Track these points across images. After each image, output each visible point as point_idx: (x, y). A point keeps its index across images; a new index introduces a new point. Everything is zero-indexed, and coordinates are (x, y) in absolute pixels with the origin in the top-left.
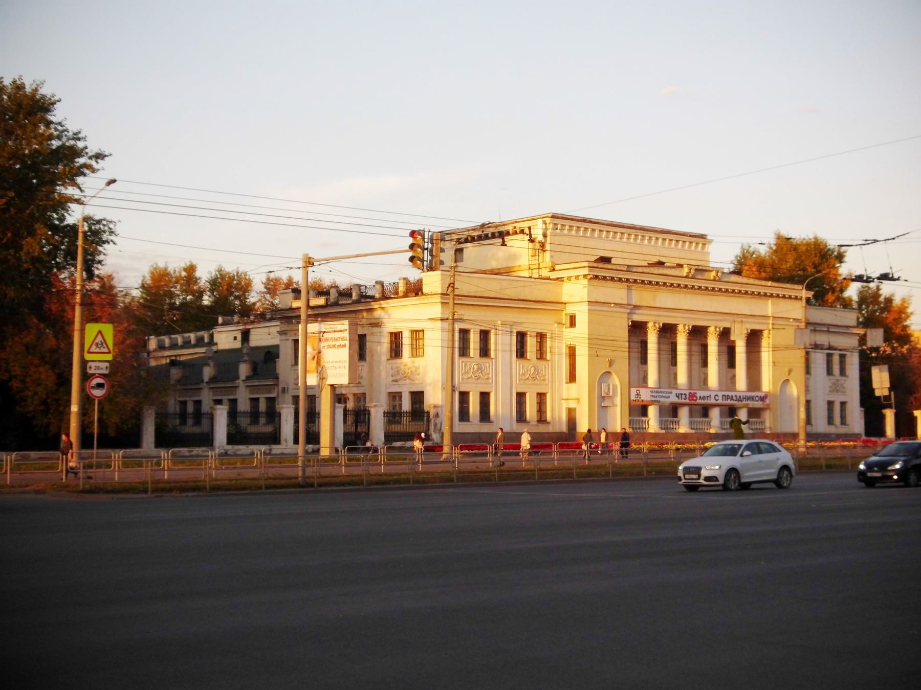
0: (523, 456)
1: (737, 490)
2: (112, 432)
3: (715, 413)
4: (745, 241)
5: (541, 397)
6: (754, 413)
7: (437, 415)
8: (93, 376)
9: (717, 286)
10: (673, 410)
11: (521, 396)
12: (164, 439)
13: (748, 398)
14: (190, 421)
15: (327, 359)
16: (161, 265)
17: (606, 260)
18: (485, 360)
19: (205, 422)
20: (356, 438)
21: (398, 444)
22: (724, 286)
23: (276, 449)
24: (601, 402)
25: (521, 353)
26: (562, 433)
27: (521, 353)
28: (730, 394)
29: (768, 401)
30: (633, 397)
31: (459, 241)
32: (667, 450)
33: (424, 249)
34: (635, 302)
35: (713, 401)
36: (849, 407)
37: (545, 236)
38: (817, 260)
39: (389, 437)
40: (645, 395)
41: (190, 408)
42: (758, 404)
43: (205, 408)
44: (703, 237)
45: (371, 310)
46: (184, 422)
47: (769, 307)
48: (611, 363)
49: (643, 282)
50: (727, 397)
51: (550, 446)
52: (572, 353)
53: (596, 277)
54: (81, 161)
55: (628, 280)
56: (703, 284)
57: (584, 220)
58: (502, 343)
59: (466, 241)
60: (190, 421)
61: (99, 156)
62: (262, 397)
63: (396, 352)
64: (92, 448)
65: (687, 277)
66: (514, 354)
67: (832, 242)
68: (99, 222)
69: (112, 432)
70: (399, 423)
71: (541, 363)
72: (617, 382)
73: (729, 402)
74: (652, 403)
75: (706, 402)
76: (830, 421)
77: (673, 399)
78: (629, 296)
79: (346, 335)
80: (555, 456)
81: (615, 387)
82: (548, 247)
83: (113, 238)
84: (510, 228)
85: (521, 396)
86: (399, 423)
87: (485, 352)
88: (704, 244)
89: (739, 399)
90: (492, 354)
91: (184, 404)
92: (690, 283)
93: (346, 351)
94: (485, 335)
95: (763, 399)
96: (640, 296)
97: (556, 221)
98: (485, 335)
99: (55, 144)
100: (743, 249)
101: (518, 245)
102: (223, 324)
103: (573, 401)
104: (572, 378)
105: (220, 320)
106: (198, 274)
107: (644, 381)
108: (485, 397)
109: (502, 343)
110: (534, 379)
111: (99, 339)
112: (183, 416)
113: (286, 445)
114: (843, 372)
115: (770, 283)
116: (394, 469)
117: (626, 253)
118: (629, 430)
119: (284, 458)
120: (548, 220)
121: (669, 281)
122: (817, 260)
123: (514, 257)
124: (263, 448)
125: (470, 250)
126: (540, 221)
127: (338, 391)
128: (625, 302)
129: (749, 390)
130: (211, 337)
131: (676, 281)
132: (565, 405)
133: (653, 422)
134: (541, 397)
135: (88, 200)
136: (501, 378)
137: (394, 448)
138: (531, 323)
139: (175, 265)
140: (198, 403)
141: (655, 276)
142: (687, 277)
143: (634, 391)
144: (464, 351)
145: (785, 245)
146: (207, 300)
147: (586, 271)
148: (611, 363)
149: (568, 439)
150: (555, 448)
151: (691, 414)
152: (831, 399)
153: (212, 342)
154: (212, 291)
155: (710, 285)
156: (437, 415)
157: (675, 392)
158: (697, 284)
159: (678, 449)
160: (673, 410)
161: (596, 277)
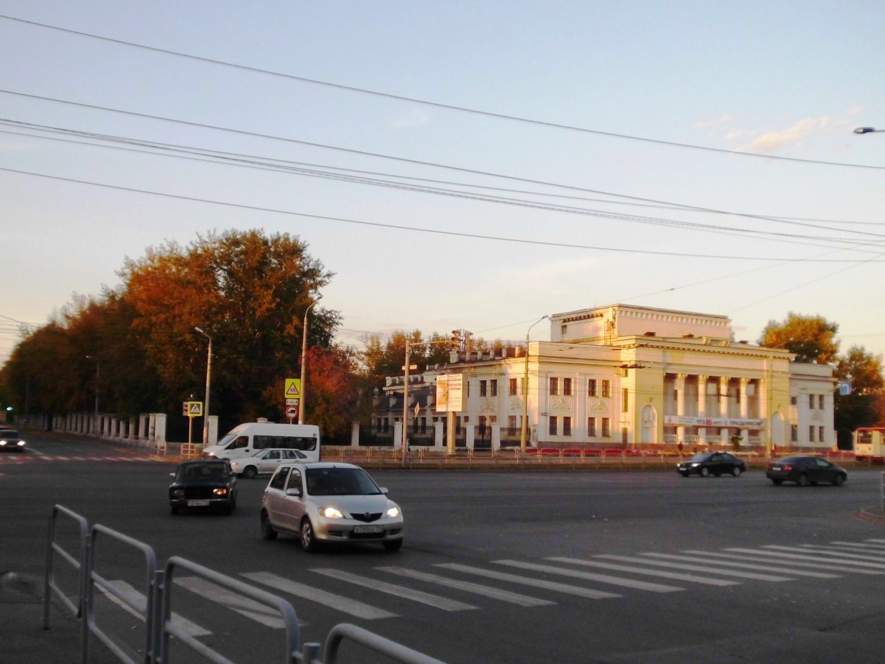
0: (470, 454)
1: (807, 486)
2: (332, 436)
3: (725, 433)
4: (772, 318)
5: (605, 421)
6: (753, 433)
7: (535, 431)
8: (289, 406)
9: (726, 350)
10: (695, 430)
11: (591, 420)
12: (365, 440)
13: (750, 423)
14: (420, 431)
15: (451, 394)
16: (400, 331)
17: (651, 334)
18: (567, 397)
19: (390, 431)
20: (483, 445)
21: (508, 448)
22: (731, 351)
23: (432, 449)
24: (643, 423)
25: (592, 393)
26: (619, 444)
27: (592, 393)
28: (736, 420)
29: (762, 425)
30: (666, 421)
31: (565, 321)
32: (659, 455)
33: (460, 340)
34: (669, 360)
35: (723, 425)
36: (825, 431)
37: (614, 318)
38: (816, 331)
39: (504, 443)
40: (675, 421)
41: (383, 423)
42: (755, 427)
43: (390, 423)
44: (724, 318)
45: (500, 365)
46: (379, 430)
47: (764, 364)
48: (651, 400)
49: (673, 348)
50: (734, 423)
51: (579, 451)
52: (626, 392)
53: (642, 346)
54: (319, 279)
55: (663, 347)
56: (716, 350)
57: (641, 308)
58: (579, 387)
59: (569, 320)
60: (420, 431)
61: (329, 275)
62: (383, 418)
63: (513, 391)
64: (187, 441)
65: (705, 345)
66: (587, 393)
67: (830, 320)
68: (330, 312)
69: (332, 436)
70: (514, 435)
71: (606, 400)
72: (655, 411)
73: (735, 425)
74: (680, 425)
75: (719, 425)
76: (812, 439)
77: (696, 424)
78: (664, 356)
79: (461, 382)
80: (582, 457)
81: (654, 415)
82: (616, 325)
83: (341, 321)
84: (594, 313)
85: (591, 420)
86: (514, 435)
87: (567, 391)
88: (726, 323)
89: (742, 424)
90: (572, 393)
91: (379, 420)
92: (707, 348)
93: (461, 391)
94: (568, 381)
95: (759, 424)
96: (671, 357)
97: (622, 309)
98: (568, 381)
99: (306, 268)
100: (770, 323)
101: (601, 322)
102: (430, 370)
103: (624, 422)
104: (626, 409)
105: (427, 368)
106: (421, 337)
107: (675, 412)
108: (567, 420)
109: (579, 387)
110: (601, 409)
111: (293, 387)
112: (379, 427)
113: (438, 447)
114: (821, 406)
115: (765, 349)
116: (474, 462)
117: (663, 330)
118: (683, 443)
119: (436, 455)
120: (616, 308)
121: (692, 347)
122: (816, 331)
123: (597, 329)
124: (424, 448)
125: (571, 326)
126: (611, 309)
127: (457, 415)
128: (661, 361)
129: (749, 417)
130: (422, 378)
131: (697, 348)
132: (622, 426)
133: (680, 437)
134: (605, 421)
135: (325, 300)
136: (579, 409)
137: (506, 450)
138: (599, 376)
139: (408, 330)
140: (386, 419)
141: (688, 343)
142: (705, 345)
143: (667, 418)
144: (553, 391)
145: (796, 323)
146: (427, 353)
147: (633, 342)
148: (651, 400)
149: (623, 447)
150: (603, 453)
151: (708, 433)
152: (812, 424)
153: (422, 382)
154: (431, 348)
155: (721, 350)
156: (535, 431)
157: (696, 418)
158: (711, 349)
159: (665, 455)
160: (695, 430)
161: (642, 346)
